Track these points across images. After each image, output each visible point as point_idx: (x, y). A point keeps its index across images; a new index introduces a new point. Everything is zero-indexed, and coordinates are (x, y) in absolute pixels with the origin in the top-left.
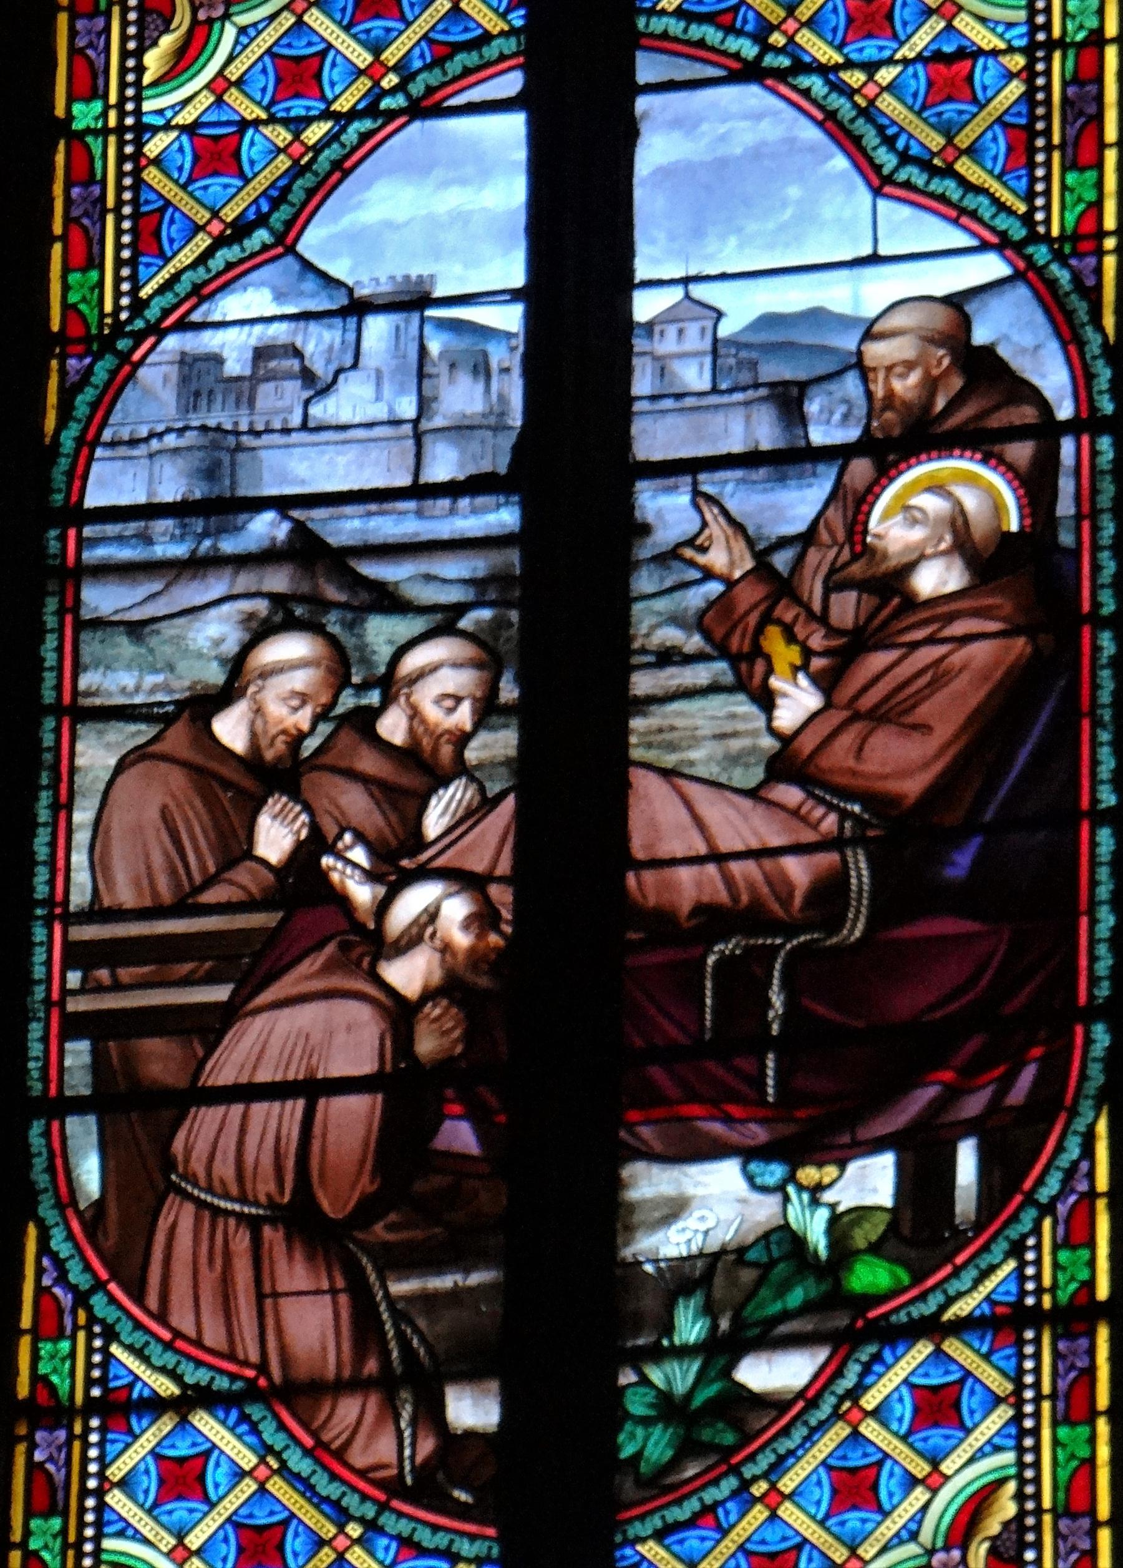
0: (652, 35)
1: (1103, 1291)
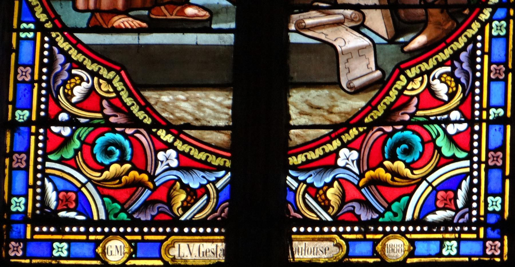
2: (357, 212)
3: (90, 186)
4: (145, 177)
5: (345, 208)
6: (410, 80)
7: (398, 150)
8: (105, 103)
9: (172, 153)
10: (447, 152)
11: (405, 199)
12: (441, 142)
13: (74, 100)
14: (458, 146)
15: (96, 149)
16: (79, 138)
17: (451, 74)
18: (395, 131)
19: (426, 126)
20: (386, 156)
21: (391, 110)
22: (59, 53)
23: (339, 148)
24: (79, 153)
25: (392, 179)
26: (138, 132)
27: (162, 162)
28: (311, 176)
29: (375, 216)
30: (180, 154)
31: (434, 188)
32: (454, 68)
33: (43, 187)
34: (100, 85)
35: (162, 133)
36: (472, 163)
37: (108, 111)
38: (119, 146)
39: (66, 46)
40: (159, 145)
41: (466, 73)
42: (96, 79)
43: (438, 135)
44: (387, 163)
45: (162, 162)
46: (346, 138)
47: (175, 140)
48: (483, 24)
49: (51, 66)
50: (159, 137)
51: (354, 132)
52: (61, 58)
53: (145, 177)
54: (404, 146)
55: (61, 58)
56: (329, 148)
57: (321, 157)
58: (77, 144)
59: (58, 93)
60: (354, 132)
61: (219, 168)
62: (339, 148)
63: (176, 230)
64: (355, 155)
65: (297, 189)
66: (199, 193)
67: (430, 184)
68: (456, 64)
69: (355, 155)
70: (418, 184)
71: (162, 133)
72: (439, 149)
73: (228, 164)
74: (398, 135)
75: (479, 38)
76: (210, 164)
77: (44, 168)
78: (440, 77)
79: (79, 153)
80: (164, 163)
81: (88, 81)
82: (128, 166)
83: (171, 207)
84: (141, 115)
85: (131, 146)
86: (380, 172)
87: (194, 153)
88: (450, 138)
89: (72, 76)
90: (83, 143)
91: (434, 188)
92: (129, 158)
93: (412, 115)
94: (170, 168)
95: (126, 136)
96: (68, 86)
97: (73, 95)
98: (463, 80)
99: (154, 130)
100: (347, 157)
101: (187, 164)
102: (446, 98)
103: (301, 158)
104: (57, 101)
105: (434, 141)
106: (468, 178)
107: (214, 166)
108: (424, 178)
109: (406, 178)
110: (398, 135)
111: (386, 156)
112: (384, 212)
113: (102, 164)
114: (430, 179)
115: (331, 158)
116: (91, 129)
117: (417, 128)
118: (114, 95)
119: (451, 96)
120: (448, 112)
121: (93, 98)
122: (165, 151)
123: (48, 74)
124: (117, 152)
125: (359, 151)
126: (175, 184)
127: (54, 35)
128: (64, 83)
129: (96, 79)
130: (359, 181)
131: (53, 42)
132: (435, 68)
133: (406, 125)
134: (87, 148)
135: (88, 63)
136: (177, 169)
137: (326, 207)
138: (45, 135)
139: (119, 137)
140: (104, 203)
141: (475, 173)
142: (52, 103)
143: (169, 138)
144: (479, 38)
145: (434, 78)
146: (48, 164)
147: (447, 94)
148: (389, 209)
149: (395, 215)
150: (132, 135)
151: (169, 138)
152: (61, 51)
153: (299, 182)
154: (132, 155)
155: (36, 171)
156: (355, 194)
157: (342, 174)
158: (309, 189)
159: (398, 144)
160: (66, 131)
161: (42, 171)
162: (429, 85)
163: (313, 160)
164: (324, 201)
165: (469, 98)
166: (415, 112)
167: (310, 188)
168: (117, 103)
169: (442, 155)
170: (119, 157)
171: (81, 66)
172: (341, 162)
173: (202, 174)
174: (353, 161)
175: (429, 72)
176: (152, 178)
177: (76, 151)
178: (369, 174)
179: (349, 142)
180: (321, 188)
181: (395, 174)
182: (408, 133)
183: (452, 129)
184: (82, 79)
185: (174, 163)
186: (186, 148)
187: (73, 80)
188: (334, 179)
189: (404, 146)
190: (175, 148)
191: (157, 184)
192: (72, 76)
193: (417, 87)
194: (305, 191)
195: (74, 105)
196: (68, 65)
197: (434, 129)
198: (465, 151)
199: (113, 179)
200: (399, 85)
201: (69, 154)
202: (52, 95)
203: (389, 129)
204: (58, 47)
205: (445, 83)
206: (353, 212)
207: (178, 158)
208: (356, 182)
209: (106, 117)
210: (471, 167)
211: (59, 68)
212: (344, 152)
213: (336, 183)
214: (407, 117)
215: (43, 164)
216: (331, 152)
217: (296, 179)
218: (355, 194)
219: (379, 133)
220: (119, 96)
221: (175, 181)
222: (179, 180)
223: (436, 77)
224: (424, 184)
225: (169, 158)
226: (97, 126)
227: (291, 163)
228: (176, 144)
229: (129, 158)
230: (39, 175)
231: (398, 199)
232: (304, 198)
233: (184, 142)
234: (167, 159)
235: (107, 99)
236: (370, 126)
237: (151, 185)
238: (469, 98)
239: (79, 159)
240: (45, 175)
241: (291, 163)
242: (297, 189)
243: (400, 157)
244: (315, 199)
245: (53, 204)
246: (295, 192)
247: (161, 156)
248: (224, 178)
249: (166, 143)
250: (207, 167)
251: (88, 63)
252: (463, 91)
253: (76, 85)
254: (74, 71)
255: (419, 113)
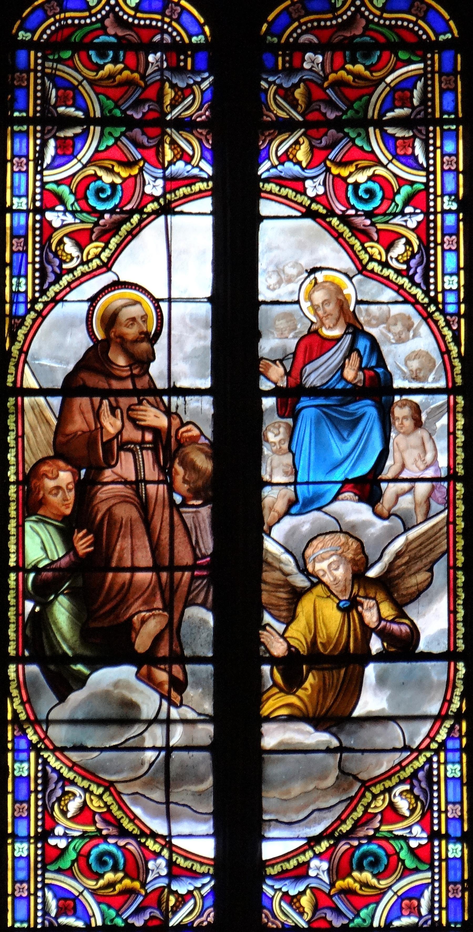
0: (266, 192)
1: (459, 69)
2: (329, 918)
3: (385, 162)
4: (335, 171)
5: (318, 915)
6: (98, 256)
7: (109, 192)
8: (375, 236)
9: (311, 193)
10: (410, 863)
11: (102, 148)
12: (403, 855)
13: (403, 240)
14: (420, 860)
15: (380, 194)
16: (397, 205)
17: (62, 262)
18: (360, 845)
19: (392, 842)
20: (354, 867)
21: (358, 824)
22: (52, 772)
23: (311, 859)
24: (76, 865)
25: (113, 166)
26: (344, 212)
27: (153, 871)
28: (188, 172)
29: (346, 922)
30: (304, 192)
31: (398, 897)
32: (60, 267)
33: (427, 159)
34: (91, 800)
35: (150, 843)
36: (433, 874)
37: (99, 825)
38: (360, 199)
39: (414, 290)
40: (325, 202)
41: (49, 263)
42: (88, 795)
43: (402, 848)
44: (118, 181)
45: (153, 871)
46: (318, 849)
47: (310, 205)
48: (33, 309)
49: (427, 269)
50: (324, 207)
51: (325, 845)
52: (418, 279)
53: (335, 171)
54: (103, 196)
55: (418, 279)
56: (302, 859)
57: (178, 189)
58: (73, 855)
59: (419, 246)
60: (325, 845)
61: (268, 180)
62: (311, 859)
63: (322, 23)
64: (325, 865)
65: (273, 897)
66: (285, 158)
67: (79, 161)
68: (58, 271)
69: (148, 190)
70: (384, 893)
71: (150, 843)
72: (403, 861)
73: (211, 871)
74: (364, 848)
75: (37, 295)
76: (277, 184)
77: (427, 176)
78: (72, 259)
79: (76, 865)
80: (155, 872)
81: (391, 258)
82: (351, 180)
83: (310, 144)
84: (342, 228)
85: (348, 199)
86: (124, 174)
87: (291, 194)
88: (411, 850)
89: (407, 262)
90: (393, 200)
91: (398, 897)
92: (350, 188)
93: (377, 830)
94: (160, 876)
95: (353, 207)
96: (409, 253)
97: (405, 244)
98: (422, 798)
99: (143, 840)
100: (319, 868)
101: (297, 183)
102: (66, 240)
103: (277, 869)
104: (53, 817)
105: (398, 854)
106: (430, 888)
107: (199, 873)
108: (390, 888)
109: (374, 887)
110: (364, 848)
111: (119, 188)
112: (120, 136)
113: (374, 182)
114: (79, 166)
115: (168, 187)
116: (87, 840)
117: (384, 843)
118: (105, 810)
119: (61, 242)
120: (410, 827)
121: (86, 813)
122: (317, 195)
123: (429, 262)
124: (361, 193)
125: (144, 193)
126: (307, 165)
127: (426, 300)
128: (59, 800)
129: (384, 259)
130: (330, 890)
131: (426, 293)
132: (397, 784)
133: (370, 839)
134: (389, 195)
135: (78, 780)
136: (306, 178)
137: (301, 914)
138: (43, 848)
139: (360, 207)
140: (100, 909)
141: (436, 885)
142: (47, 817)
143: (314, 207)
144: (37, 295)
145: (78, 257)
146: (424, 180)
147: (64, 244)
148: (117, 139)
149: (110, 134)
150: (124, 847)
151: (314, 207)
152: (418, 286)
153: (276, 890)
154: (347, 191)
155: (434, 173)
156: (326, 902)
157: (159, 172)
158: (188, 159)
159: (365, 855)
160: (62, 844)
161: (428, 173)
162: (82, 250)
163: (186, 186)
164: (175, 148)
165: (428, 815)
166: (379, 828)
167: (188, 159)
168: (108, 817)
169: (405, 868)
170: (359, 188)
171: (398, 272)
172: (312, 873)
173: (282, 174)
174: (323, 872)
175: (389, 790)
176: (144, 885)
177: (73, 862)
178: (340, 884)
179: (320, 854)
180: (178, 160)
181: (110, 171)
182: (373, 847)
183: (414, 844)
184: (397, 259)
185: (308, 183)
186: (300, 198)
187: (405, 259)
188: (307, 887)
189: (103, 196)
190: (309, 198)
191: (148, 891)
192: (407, 262)
193: (380, 804)
194: (282, 899)
195: (403, 236)
196: (411, 272)
197: (397, 844)
198: (48, 190)
199: (364, 168)
200: (365, 801)
201: (406, 190)
202: (47, 812)
203: (355, 843)
204: (51, 767)
205: (67, 254)
206: (325, 918)
207: (305, 189)
208: (327, 891)
209: (100, 830)
210: (432, 878)
211: (419, 270)
212: (158, 192)
213: (308, 891)
214: (371, 832)
215: (428, 180)
216: (304, 863)
217: (272, 887)
218: (326, 902)
219: (347, 846)
220: (109, 811)
221: (306, 168)
222: (303, 169)
223: (75, 259)
224: (84, 161)
225: (313, 188)
226: (92, 838)
227: (268, 873)
228: (309, 202)
229: (350, 188)
230: (431, 169)
231: (108, 147)
232: (193, 150)
233: (301, 204)
234: (158, 868)
235: (372, 240)
236: (338, 840)
237: (328, 163)
238: (428, 815)
239: (396, 187)
240: (426, 170)
241: (268, 873)
242: (200, 160)
243: (108, 186)
244: (183, 150)
245: (418, 144)
246: (272, 899)
247: (321, 190)
248: (264, 170)
249: (318, 203)
250: (279, 180)
251: (78, 780)
252: (50, 245)
253: (402, 255)
254: (404, 267)
255: (384, 828)
